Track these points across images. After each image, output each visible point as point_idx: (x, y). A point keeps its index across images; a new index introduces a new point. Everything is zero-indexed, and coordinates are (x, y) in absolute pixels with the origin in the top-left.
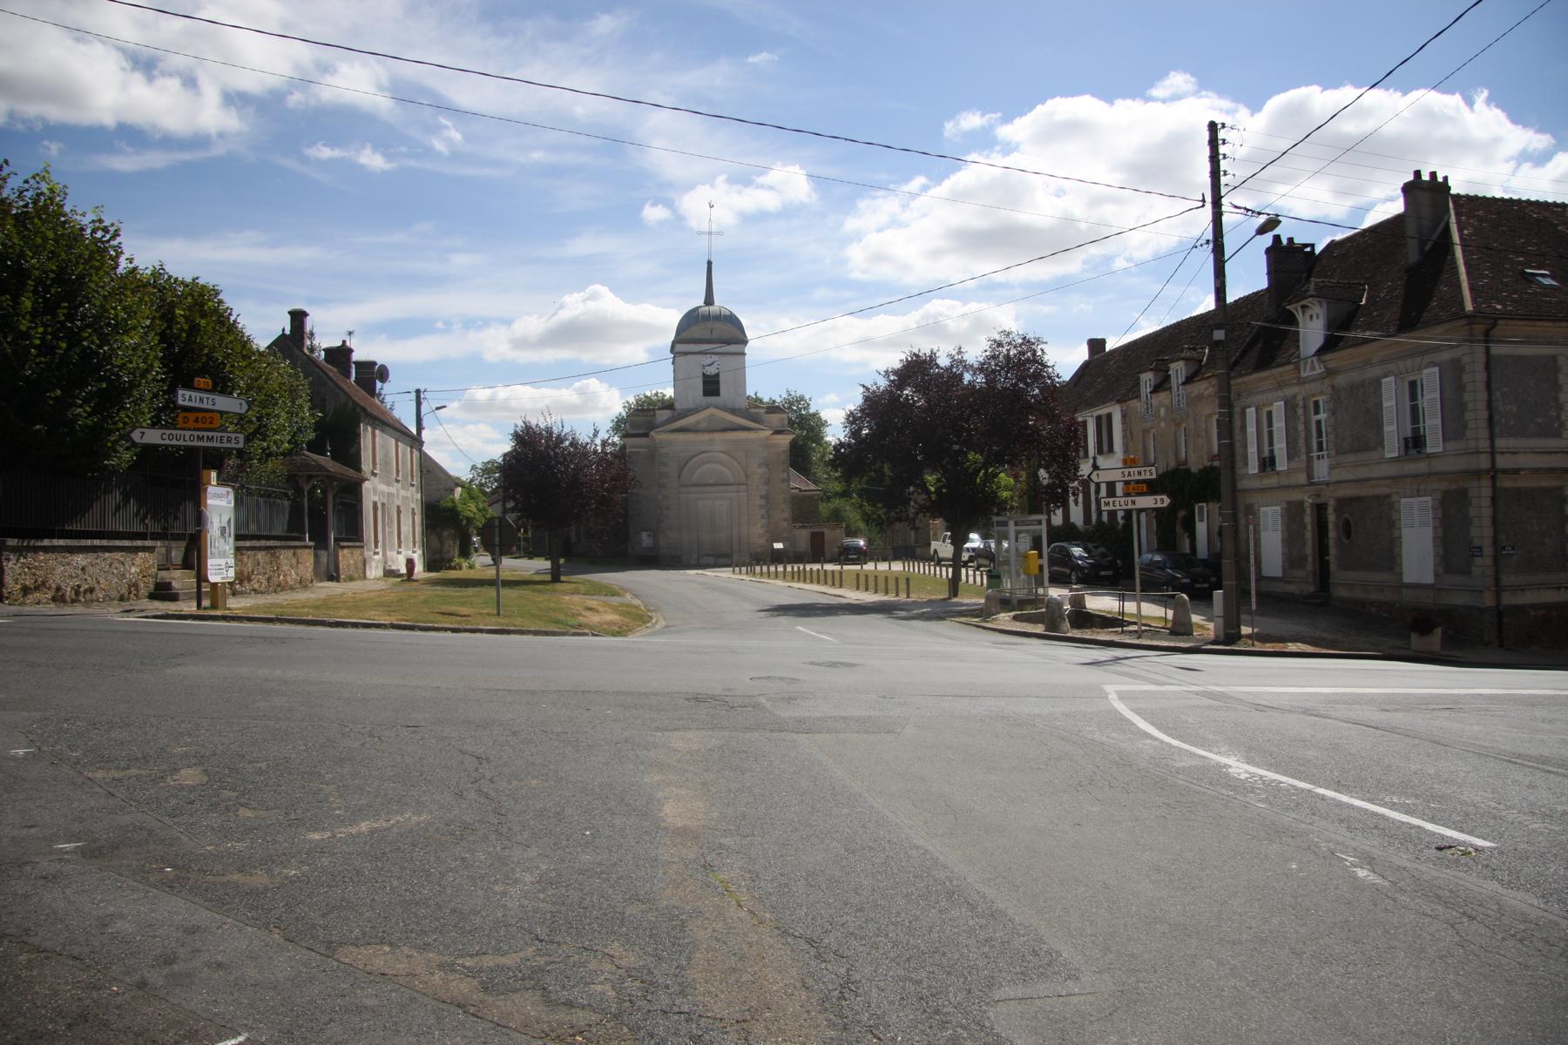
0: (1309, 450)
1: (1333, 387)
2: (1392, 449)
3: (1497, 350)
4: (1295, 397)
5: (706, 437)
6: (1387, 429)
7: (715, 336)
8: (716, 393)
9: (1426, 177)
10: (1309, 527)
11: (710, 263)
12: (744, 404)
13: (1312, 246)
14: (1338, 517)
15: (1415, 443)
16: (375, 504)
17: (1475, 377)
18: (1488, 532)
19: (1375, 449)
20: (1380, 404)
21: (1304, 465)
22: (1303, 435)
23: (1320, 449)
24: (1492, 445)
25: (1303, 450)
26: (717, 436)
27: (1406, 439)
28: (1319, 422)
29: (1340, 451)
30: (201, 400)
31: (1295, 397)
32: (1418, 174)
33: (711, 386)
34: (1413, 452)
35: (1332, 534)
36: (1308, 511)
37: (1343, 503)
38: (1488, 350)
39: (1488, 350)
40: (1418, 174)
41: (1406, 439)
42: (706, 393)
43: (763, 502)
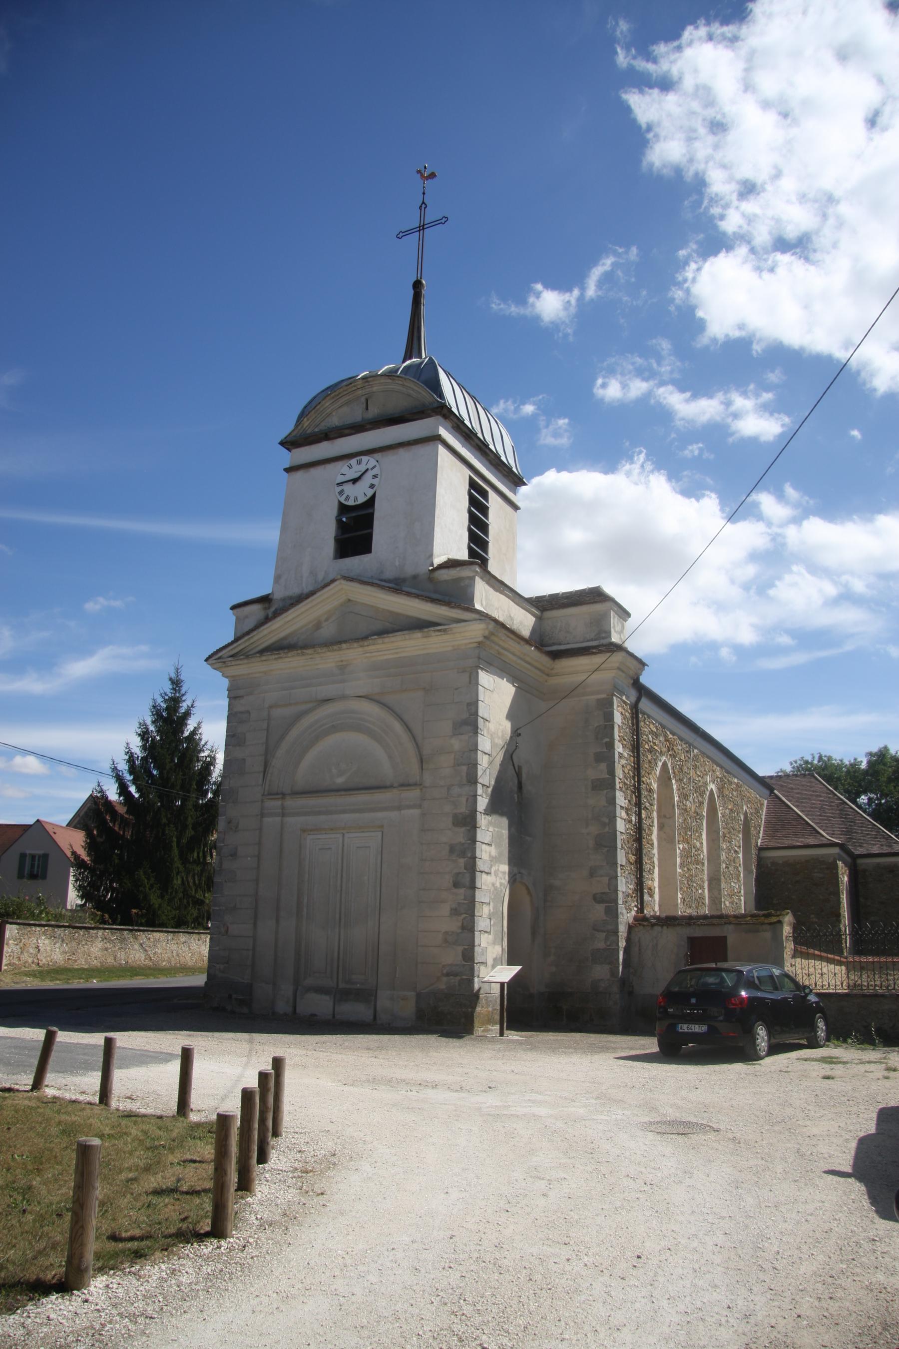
5: (327, 661)
7: (374, 411)
12: (423, 569)
26: (354, 654)
33: (355, 530)
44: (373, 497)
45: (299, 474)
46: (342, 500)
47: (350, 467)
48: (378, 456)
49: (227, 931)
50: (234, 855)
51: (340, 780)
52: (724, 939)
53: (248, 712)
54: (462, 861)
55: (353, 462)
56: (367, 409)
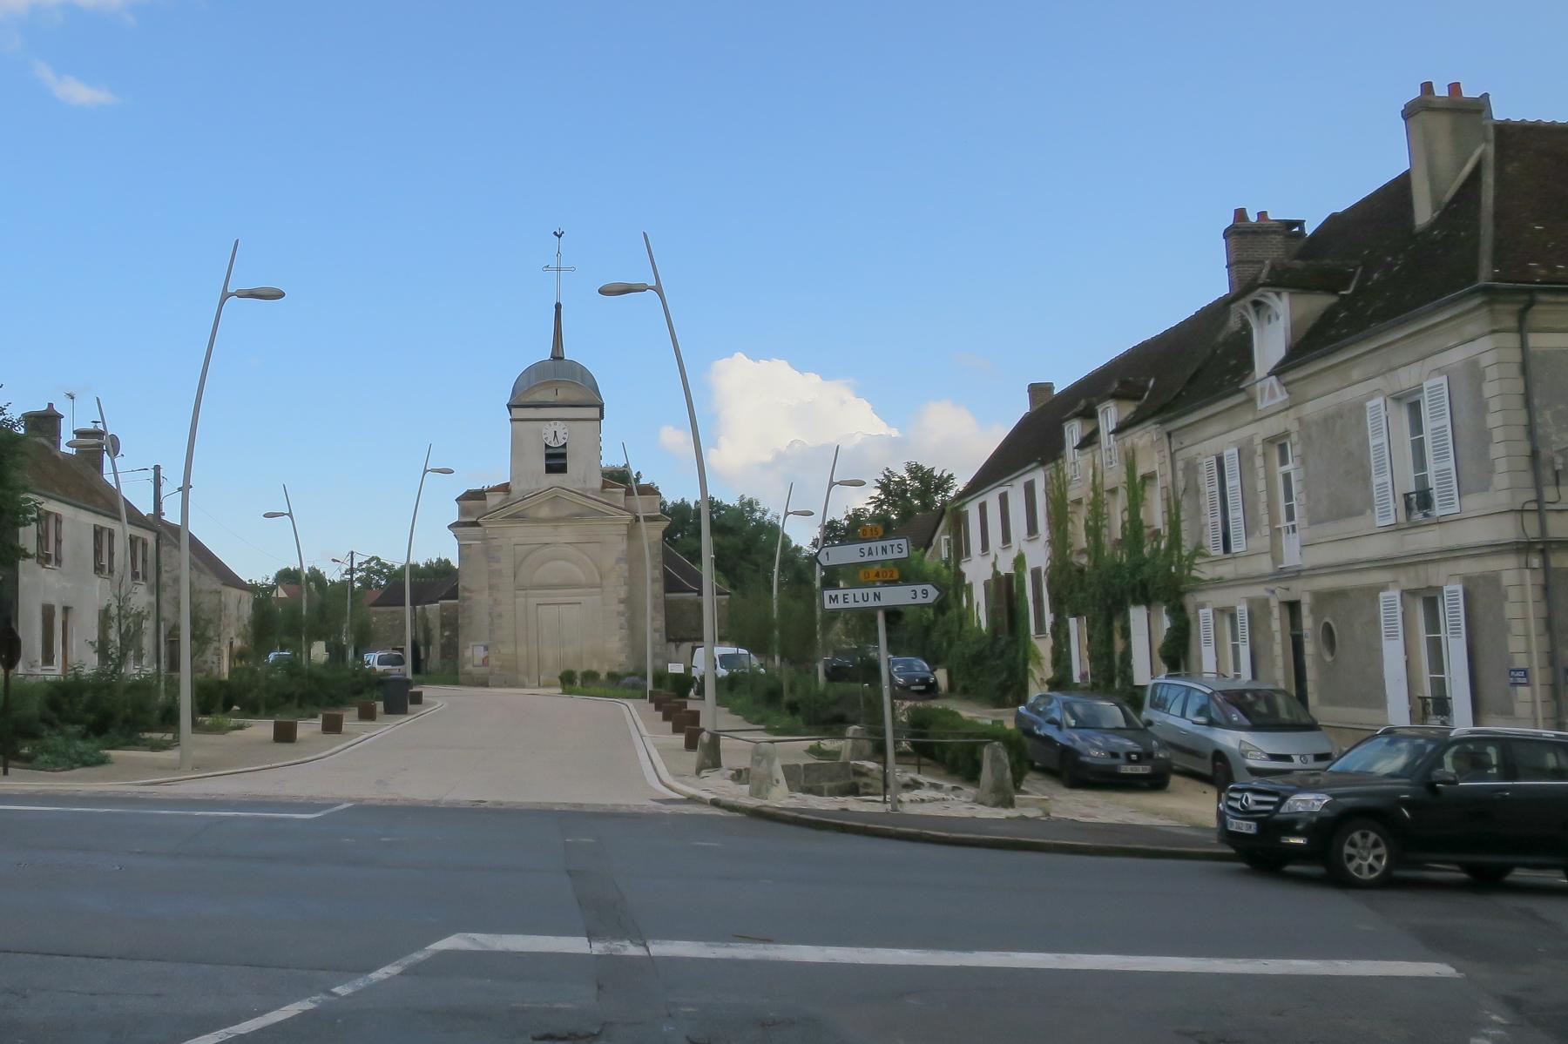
0: (1273, 519)
1: (1300, 420)
2: (1387, 511)
3: (1537, 341)
4: (1251, 440)
6: (1376, 480)
8: (562, 469)
9: (1441, 91)
10: (1278, 637)
11: (558, 307)
13: (1300, 223)
14: (1316, 622)
15: (1421, 500)
16: (48, 613)
17: (1500, 388)
18: (1538, 644)
19: (1361, 513)
20: (1365, 442)
21: (1267, 542)
22: (1263, 497)
23: (1290, 517)
24: (1539, 500)
25: (1265, 519)
27: (1406, 496)
28: (1287, 477)
29: (1315, 520)
30: (884, 550)
31: (1251, 440)
32: (1427, 87)
33: (556, 461)
34: (1418, 516)
35: (1309, 648)
36: (1276, 612)
37: (1323, 599)
38: (1523, 345)
39: (1523, 345)
40: (1427, 87)
41: (1406, 496)
42: (550, 469)
43: (622, 607)
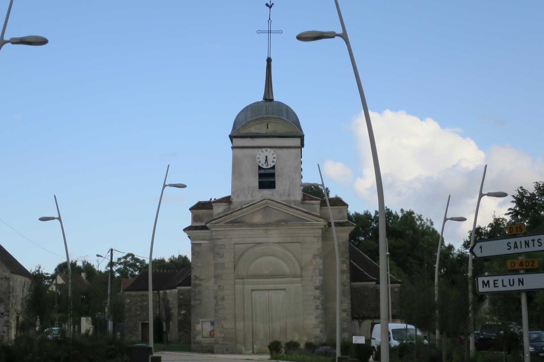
11: (269, 61)
33: (267, 179)
43: (317, 293)
44: (274, 166)
45: (238, 151)
46: (260, 165)
47: (262, 152)
48: (276, 150)
49: (223, 327)
50: (223, 299)
51: (266, 272)
52: (392, 330)
53: (224, 245)
54: (318, 301)
55: (264, 150)
56: (268, 128)
